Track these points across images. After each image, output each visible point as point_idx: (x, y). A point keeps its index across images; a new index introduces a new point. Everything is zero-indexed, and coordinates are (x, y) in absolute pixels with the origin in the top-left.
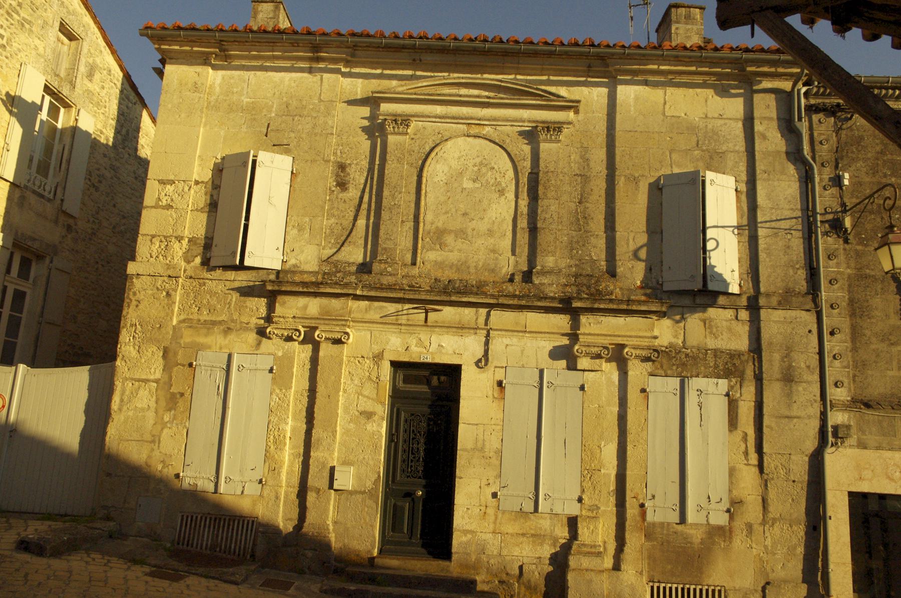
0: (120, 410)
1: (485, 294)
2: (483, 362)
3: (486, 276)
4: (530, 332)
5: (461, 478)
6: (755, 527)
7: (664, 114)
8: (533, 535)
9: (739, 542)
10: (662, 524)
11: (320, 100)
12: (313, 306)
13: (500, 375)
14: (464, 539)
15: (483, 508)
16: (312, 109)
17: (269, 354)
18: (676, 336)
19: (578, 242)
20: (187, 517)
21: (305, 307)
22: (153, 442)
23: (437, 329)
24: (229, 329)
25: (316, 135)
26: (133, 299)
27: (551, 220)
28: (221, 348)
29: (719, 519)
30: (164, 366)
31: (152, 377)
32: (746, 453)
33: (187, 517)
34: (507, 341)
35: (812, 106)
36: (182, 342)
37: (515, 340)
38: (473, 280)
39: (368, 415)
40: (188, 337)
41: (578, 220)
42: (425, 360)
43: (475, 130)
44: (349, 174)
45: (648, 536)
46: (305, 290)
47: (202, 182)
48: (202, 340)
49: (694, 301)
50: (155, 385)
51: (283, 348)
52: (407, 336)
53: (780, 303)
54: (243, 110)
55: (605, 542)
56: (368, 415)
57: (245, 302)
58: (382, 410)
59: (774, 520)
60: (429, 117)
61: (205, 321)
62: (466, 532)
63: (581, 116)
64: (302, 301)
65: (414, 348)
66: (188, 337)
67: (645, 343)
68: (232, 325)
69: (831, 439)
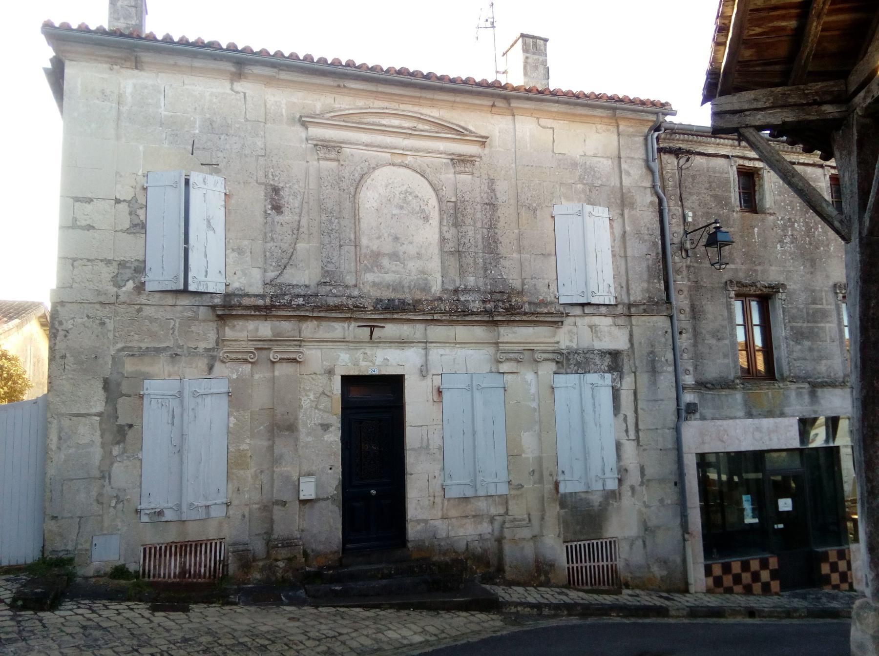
0: (59, 448)
1: (423, 312)
2: (424, 372)
3: (419, 295)
4: (459, 343)
5: (411, 474)
6: (638, 488)
7: (553, 151)
8: (474, 516)
9: (627, 500)
10: (571, 493)
11: (247, 120)
12: (265, 329)
13: (437, 381)
14: (419, 527)
15: (432, 499)
16: (239, 128)
17: (224, 377)
18: (571, 341)
19: (490, 263)
20: (150, 549)
21: (257, 330)
22: (103, 477)
23: (381, 344)
24: (176, 355)
25: (246, 156)
26: (60, 329)
27: (469, 244)
28: (170, 375)
29: (612, 485)
30: (107, 398)
31: (93, 411)
32: (627, 431)
33: (150, 549)
34: (441, 351)
35: (662, 148)
36: (125, 372)
37: (448, 351)
38: (409, 299)
39: (326, 427)
40: (130, 366)
41: (490, 244)
42: (373, 373)
43: (398, 160)
44: (283, 197)
45: (562, 505)
46: (257, 313)
47: (124, 201)
48: (145, 369)
49: (583, 311)
50: (98, 418)
51: (237, 371)
52: (355, 352)
53: (645, 310)
54: (162, 124)
55: (529, 515)
56: (326, 427)
57: (190, 327)
58: (336, 421)
59: (648, 480)
60: (356, 144)
61: (147, 348)
62: (418, 522)
63: (487, 151)
64: (251, 325)
65: (363, 364)
66: (130, 366)
67: (550, 348)
68: (179, 351)
69: (684, 414)
